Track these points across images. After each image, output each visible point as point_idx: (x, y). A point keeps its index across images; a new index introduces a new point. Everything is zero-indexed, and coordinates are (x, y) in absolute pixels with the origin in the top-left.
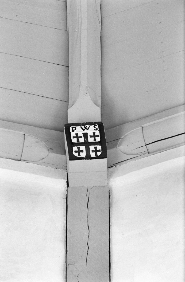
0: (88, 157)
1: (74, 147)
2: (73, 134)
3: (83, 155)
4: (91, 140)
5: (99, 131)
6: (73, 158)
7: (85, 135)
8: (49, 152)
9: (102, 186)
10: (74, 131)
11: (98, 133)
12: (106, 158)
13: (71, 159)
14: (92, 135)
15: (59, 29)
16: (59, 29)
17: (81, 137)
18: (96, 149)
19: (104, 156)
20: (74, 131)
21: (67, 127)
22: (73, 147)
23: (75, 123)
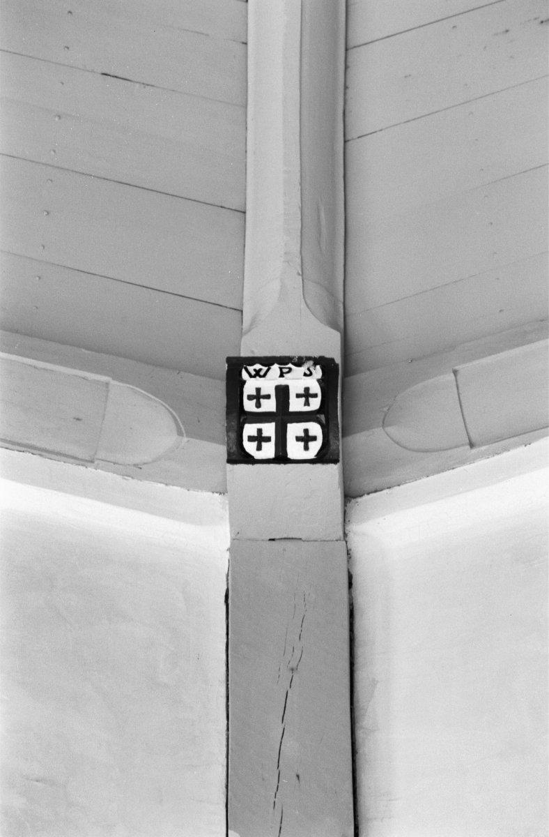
0: (281, 457)
1: (291, 422)
2: (250, 386)
3: (269, 450)
4: (296, 405)
5: (318, 380)
6: (239, 456)
7: (283, 392)
8: (180, 433)
9: (350, 577)
10: (283, 377)
11: (316, 388)
12: (335, 461)
13: (231, 461)
14: (254, 393)
15: (222, 207)
16: (222, 207)
17: (268, 397)
18: (254, 437)
19: (324, 457)
20: (283, 377)
21: (236, 367)
22: (289, 425)
23: (281, 355)
